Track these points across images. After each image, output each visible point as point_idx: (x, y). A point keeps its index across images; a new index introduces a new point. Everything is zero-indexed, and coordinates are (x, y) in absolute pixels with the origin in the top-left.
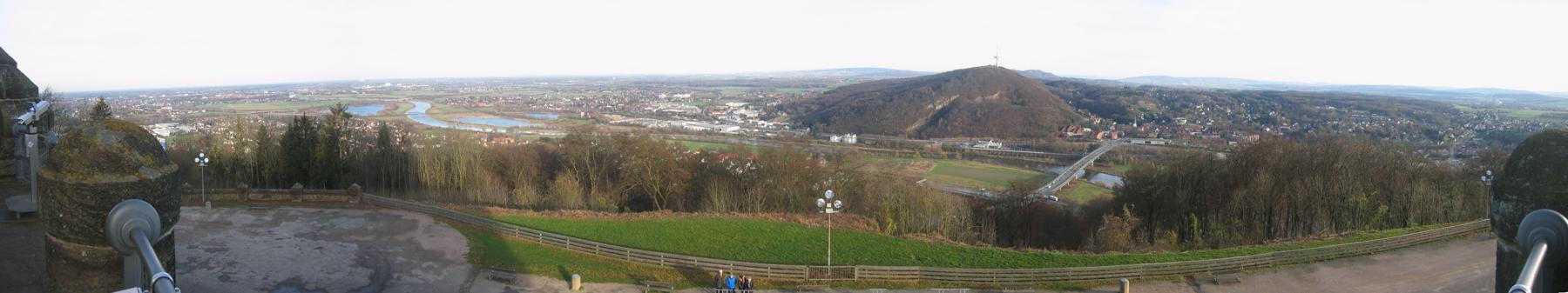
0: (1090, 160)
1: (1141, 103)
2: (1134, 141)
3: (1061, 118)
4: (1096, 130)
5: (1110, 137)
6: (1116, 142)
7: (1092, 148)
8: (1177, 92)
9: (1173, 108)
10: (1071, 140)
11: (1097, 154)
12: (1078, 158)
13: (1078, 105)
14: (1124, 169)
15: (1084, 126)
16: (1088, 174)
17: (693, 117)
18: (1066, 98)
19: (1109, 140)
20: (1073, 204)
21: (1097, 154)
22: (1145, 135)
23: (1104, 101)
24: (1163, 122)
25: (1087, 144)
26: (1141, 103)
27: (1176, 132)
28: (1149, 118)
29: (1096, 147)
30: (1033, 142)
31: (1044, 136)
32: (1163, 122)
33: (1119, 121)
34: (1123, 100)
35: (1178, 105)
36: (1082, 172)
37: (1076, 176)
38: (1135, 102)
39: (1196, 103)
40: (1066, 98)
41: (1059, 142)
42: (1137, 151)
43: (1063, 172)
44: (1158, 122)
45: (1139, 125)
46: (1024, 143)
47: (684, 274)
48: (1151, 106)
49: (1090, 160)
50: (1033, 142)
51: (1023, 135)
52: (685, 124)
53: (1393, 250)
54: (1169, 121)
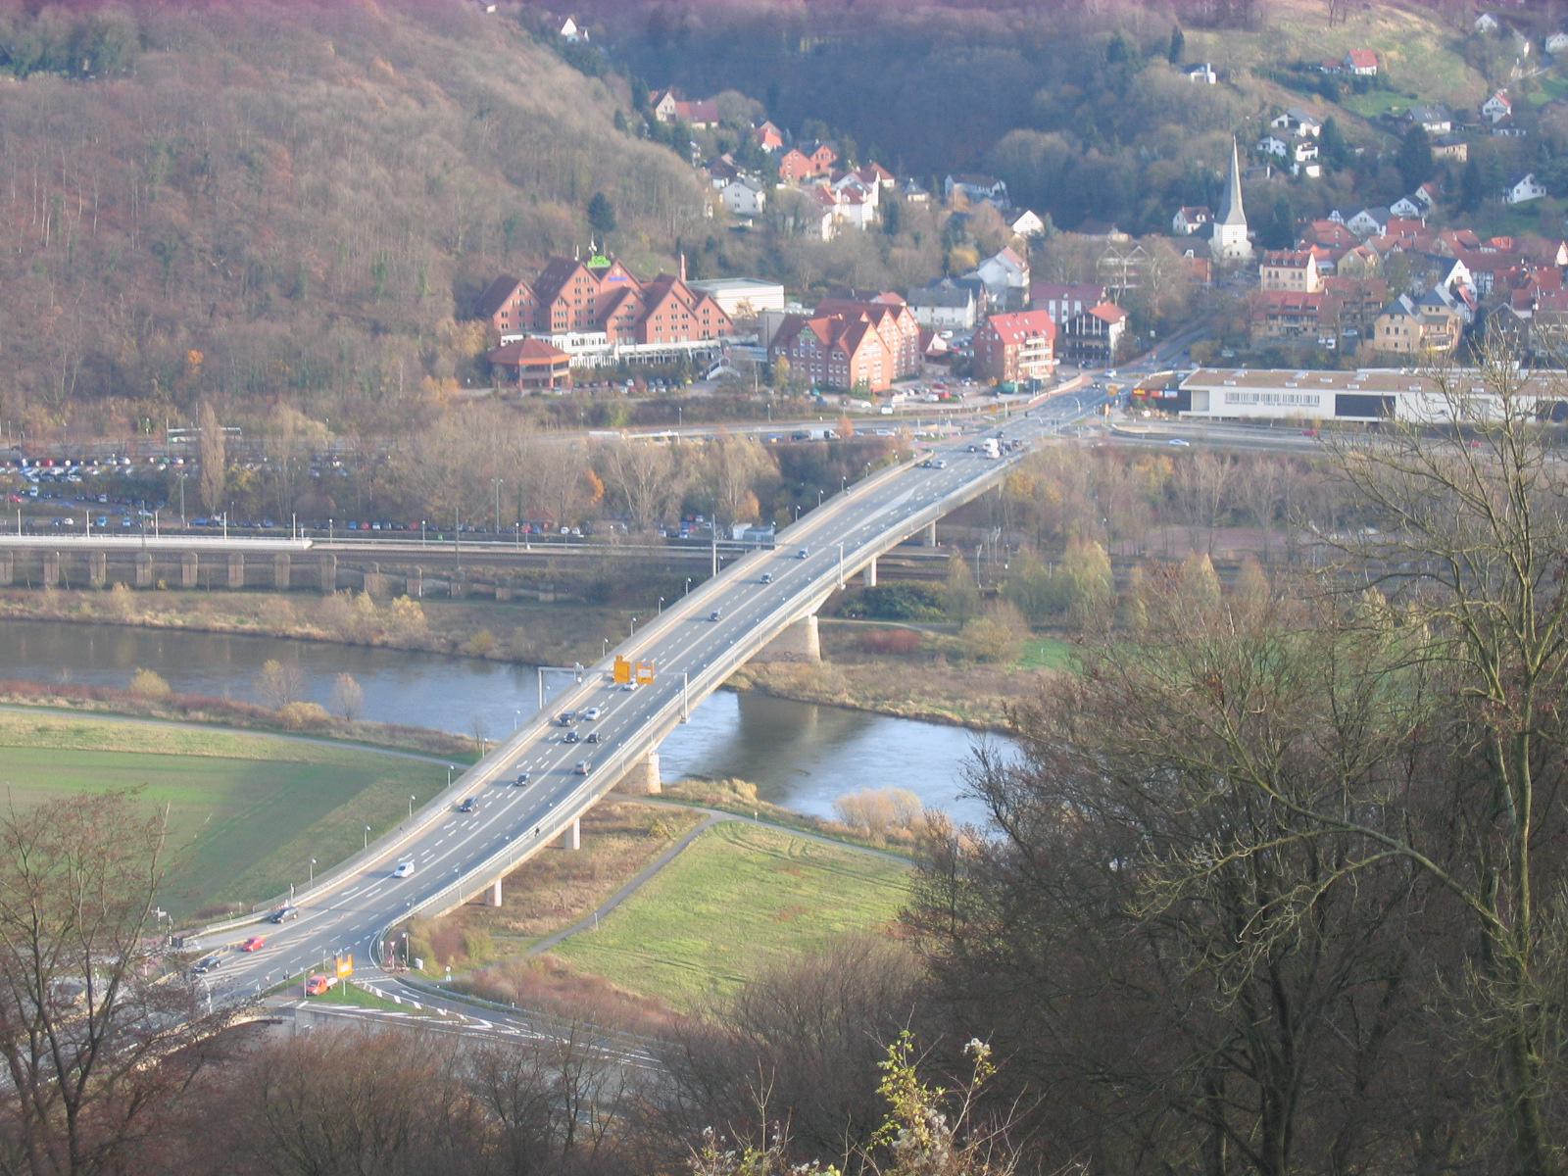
0: (777, 597)
2: (1225, 397)
3: (496, 198)
4: (841, 300)
5: (976, 363)
6: (1048, 418)
7: (802, 482)
10: (591, 401)
11: (852, 537)
15: (712, 257)
16: (771, 735)
17: (416, 752)
20: (579, 1014)
22: (1336, 337)
25: (748, 447)
28: (1386, 164)
30: (205, 439)
31: (305, 378)
33: (1075, 202)
36: (706, 716)
41: (462, 432)
42: (1240, 499)
43: (517, 729)
44: (1470, 195)
45: (1275, 233)
46: (115, 454)
49: (777, 597)
50: (205, 439)
51: (103, 380)
53: (659, 869)
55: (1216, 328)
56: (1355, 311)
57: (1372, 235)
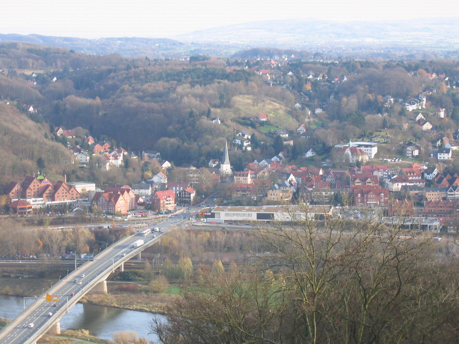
0: (95, 274)
1: (243, 102)
2: (224, 215)
4: (112, 187)
5: (152, 205)
7: (101, 241)
8: (349, 66)
9: (337, 115)
10: (38, 218)
11: (114, 258)
12: (59, 272)
13: (56, 115)
14: (173, 294)
15: (74, 175)
16: (93, 316)
18: (21, 100)
19: (154, 214)
21: (114, 258)
22: (256, 196)
23: (131, 100)
24: (308, 154)
25: (85, 231)
26: (243, 102)
27: (349, 184)
28: (270, 146)
29: (116, 234)
32: (308, 154)
33: (180, 158)
34: (189, 96)
35: (351, 103)
36: (74, 310)
37: (58, 323)
38: (224, 102)
39: (406, 96)
40: (21, 100)
42: (229, 244)
44: (294, 155)
45: (238, 167)
47: (405, 68)
48: (271, 110)
49: (95, 274)
52: (315, 332)
54: (325, 151)
55: (221, 194)
56: (262, 189)
57: (266, 167)
